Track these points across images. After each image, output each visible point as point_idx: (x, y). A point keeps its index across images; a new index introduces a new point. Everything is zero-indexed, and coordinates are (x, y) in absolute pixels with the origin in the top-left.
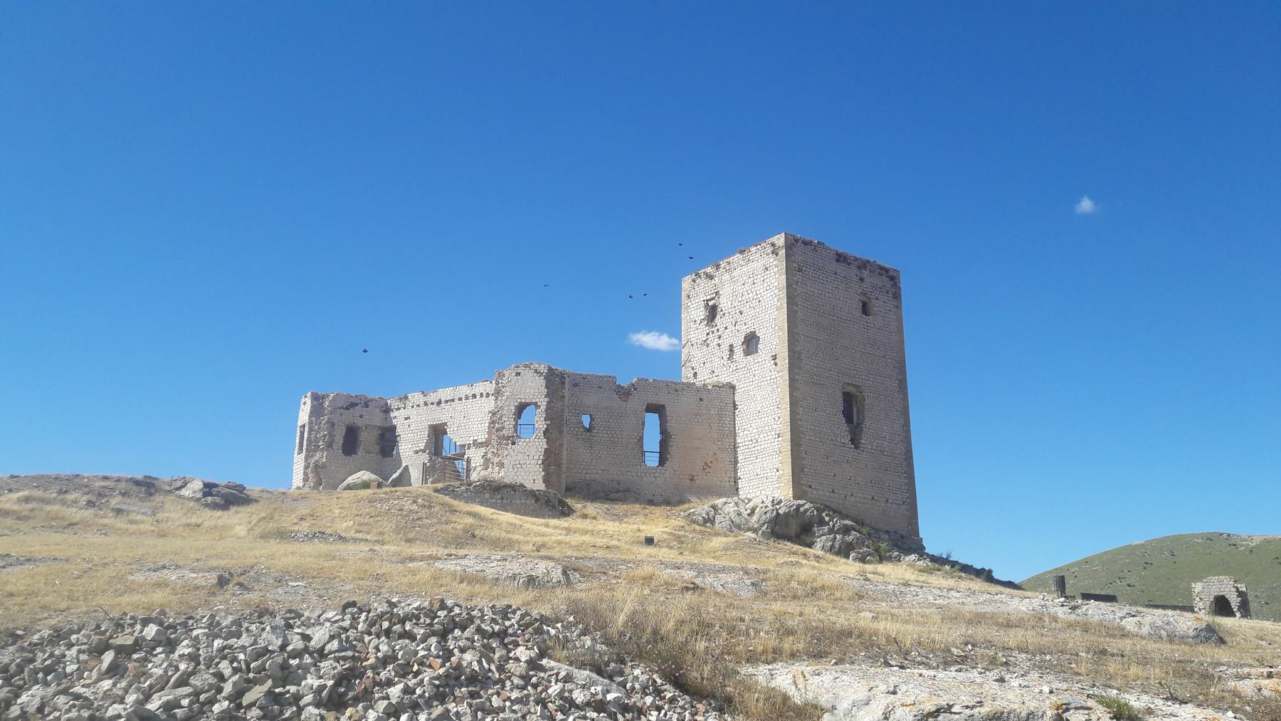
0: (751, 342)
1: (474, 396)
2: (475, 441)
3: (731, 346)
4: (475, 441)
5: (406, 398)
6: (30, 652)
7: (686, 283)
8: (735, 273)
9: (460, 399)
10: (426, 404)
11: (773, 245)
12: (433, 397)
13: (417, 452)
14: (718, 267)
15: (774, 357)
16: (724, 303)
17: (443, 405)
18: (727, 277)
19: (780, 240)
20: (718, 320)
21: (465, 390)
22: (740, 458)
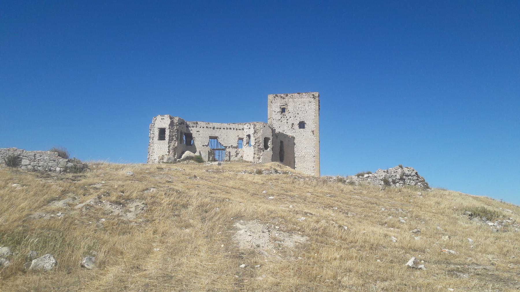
0: (302, 125)
1: (230, 129)
2: (232, 146)
3: (293, 124)
4: (232, 146)
5: (197, 123)
6: (214, 222)
7: (270, 97)
8: (295, 100)
9: (224, 129)
10: (207, 127)
11: (313, 95)
12: (211, 125)
13: (203, 146)
14: (287, 95)
15: (313, 132)
16: (290, 108)
17: (216, 129)
18: (291, 100)
19: (316, 94)
20: (286, 113)
21: (225, 125)
22: (296, 161)
